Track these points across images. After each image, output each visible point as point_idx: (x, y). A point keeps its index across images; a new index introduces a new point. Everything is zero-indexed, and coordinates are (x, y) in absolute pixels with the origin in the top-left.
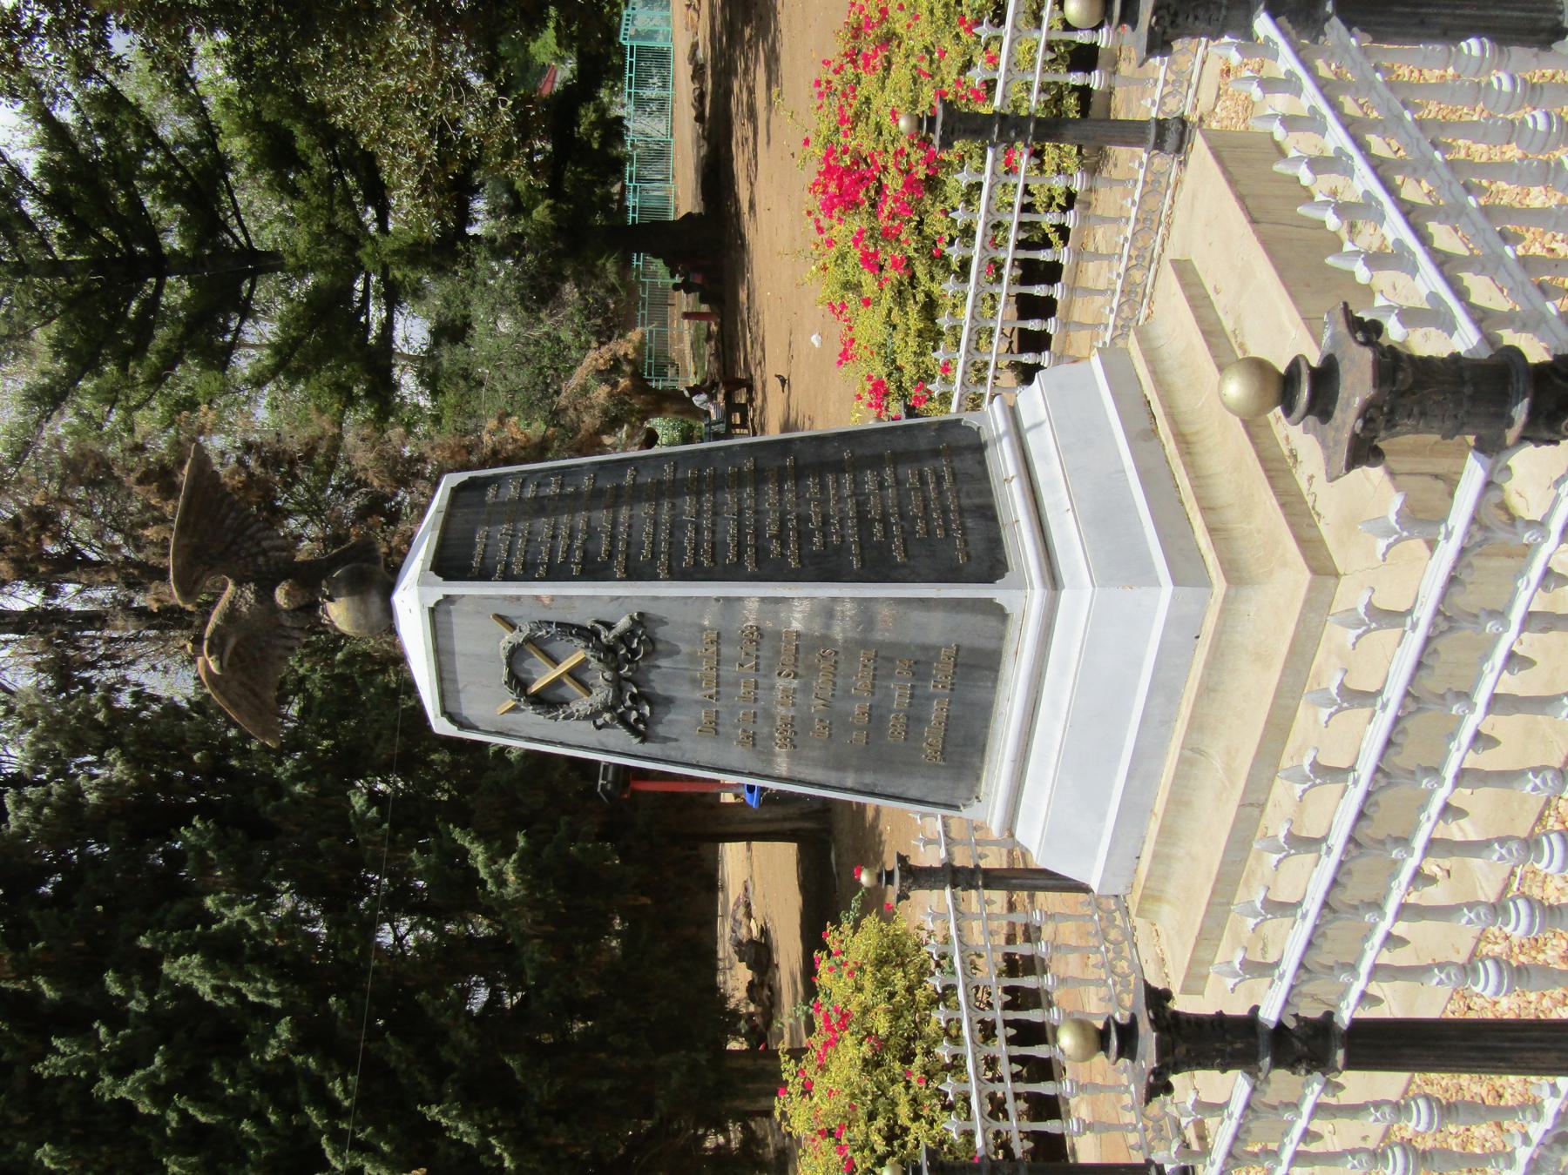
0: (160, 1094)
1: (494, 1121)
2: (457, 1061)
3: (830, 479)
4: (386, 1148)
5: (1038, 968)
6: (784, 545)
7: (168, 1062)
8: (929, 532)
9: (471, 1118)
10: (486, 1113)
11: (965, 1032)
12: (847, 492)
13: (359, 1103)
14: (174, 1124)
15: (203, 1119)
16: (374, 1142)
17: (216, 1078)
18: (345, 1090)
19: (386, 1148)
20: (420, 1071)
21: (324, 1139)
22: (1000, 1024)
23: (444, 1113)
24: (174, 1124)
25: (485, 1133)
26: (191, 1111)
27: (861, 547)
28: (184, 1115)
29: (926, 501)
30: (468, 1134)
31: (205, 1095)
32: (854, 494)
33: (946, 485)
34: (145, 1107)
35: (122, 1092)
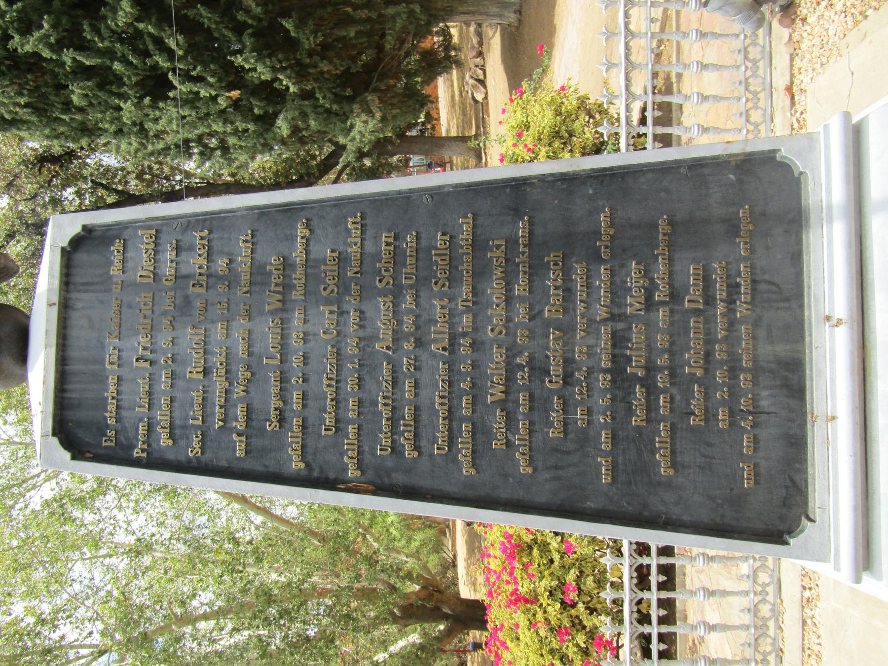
0: (57, 47)
1: (280, 62)
2: (250, 21)
3: (579, 269)
4: (211, 80)
5: (674, 143)
6: (510, 421)
7: (54, 26)
8: (709, 415)
9: (264, 63)
10: (274, 59)
11: (626, 579)
12: (601, 313)
13: (187, 53)
14: (69, 64)
15: (88, 63)
16: (204, 74)
17: (89, 37)
18: (178, 44)
19: (211, 80)
20: (227, 27)
21: (170, 75)
22: (654, 570)
23: (246, 60)
24: (69, 64)
25: (274, 69)
26: (78, 58)
27: (614, 437)
28: (74, 59)
29: (710, 341)
30: (264, 74)
31: (83, 47)
32: (613, 317)
33: (742, 310)
34: (46, 54)
35: (28, 48)
